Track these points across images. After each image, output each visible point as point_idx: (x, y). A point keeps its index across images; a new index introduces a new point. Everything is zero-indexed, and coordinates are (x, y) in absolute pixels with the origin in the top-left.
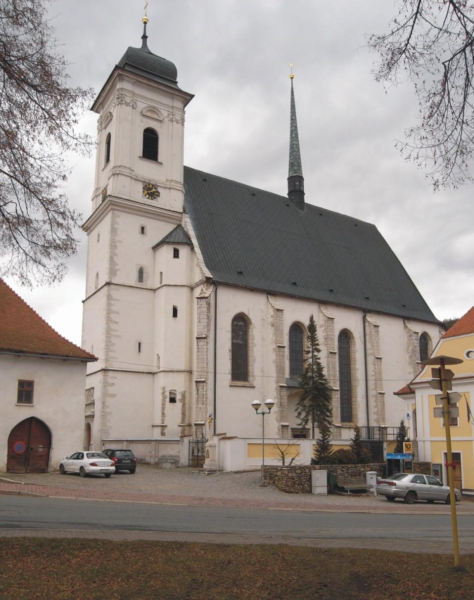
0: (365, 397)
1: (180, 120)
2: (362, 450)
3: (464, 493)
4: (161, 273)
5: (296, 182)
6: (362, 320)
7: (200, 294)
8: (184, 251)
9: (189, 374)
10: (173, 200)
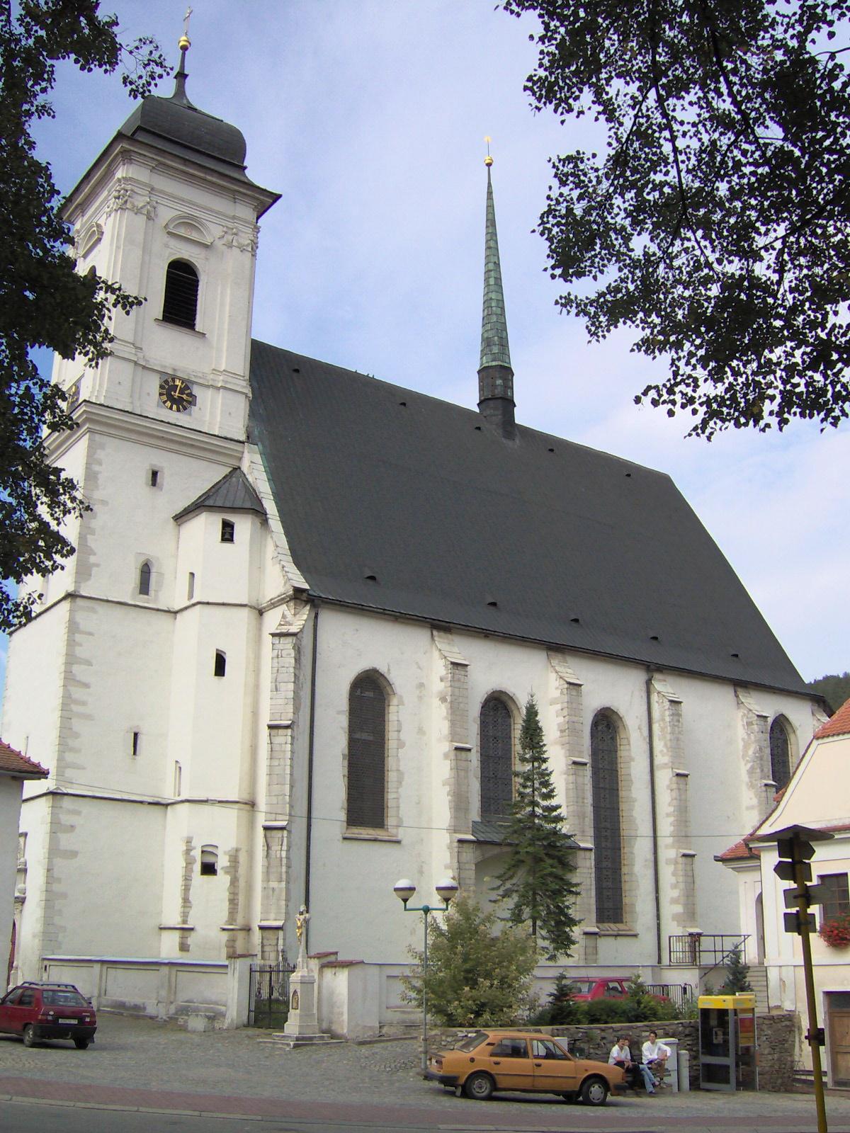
0: (652, 865)
1: (248, 245)
4: (192, 574)
5: (497, 381)
6: (644, 689)
7: (280, 625)
8: (244, 526)
9: (247, 807)
10: (223, 411)
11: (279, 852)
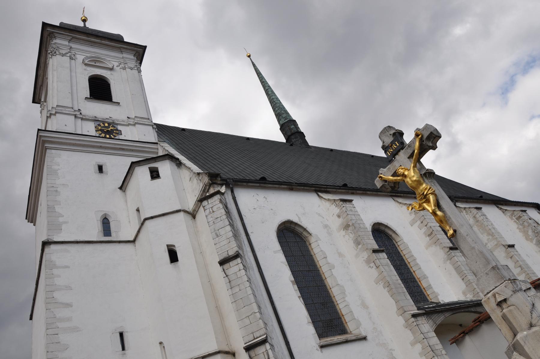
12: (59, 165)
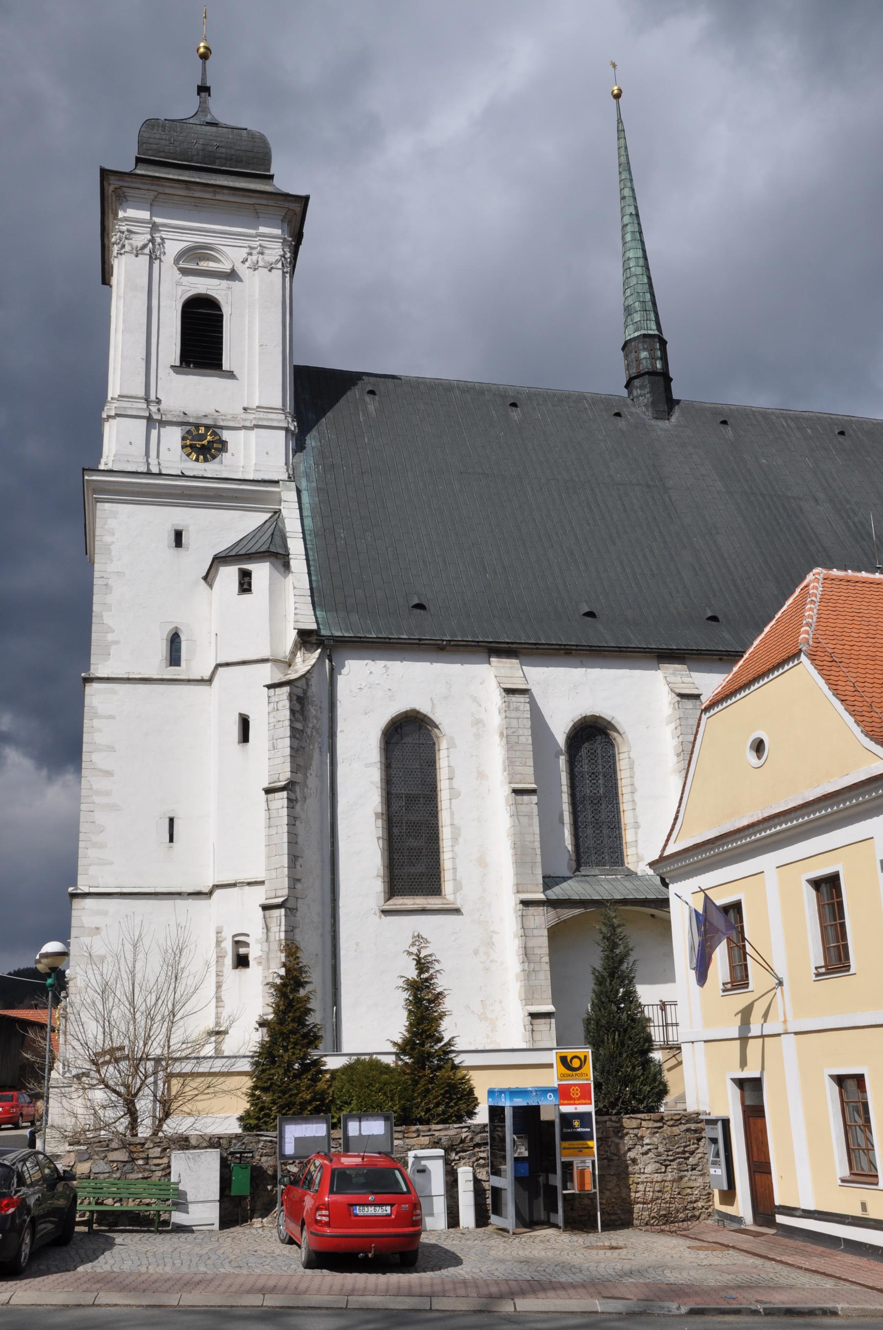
2: (455, 1067)
3: (780, 1219)
10: (258, 452)
11: (277, 934)
12: (113, 534)
